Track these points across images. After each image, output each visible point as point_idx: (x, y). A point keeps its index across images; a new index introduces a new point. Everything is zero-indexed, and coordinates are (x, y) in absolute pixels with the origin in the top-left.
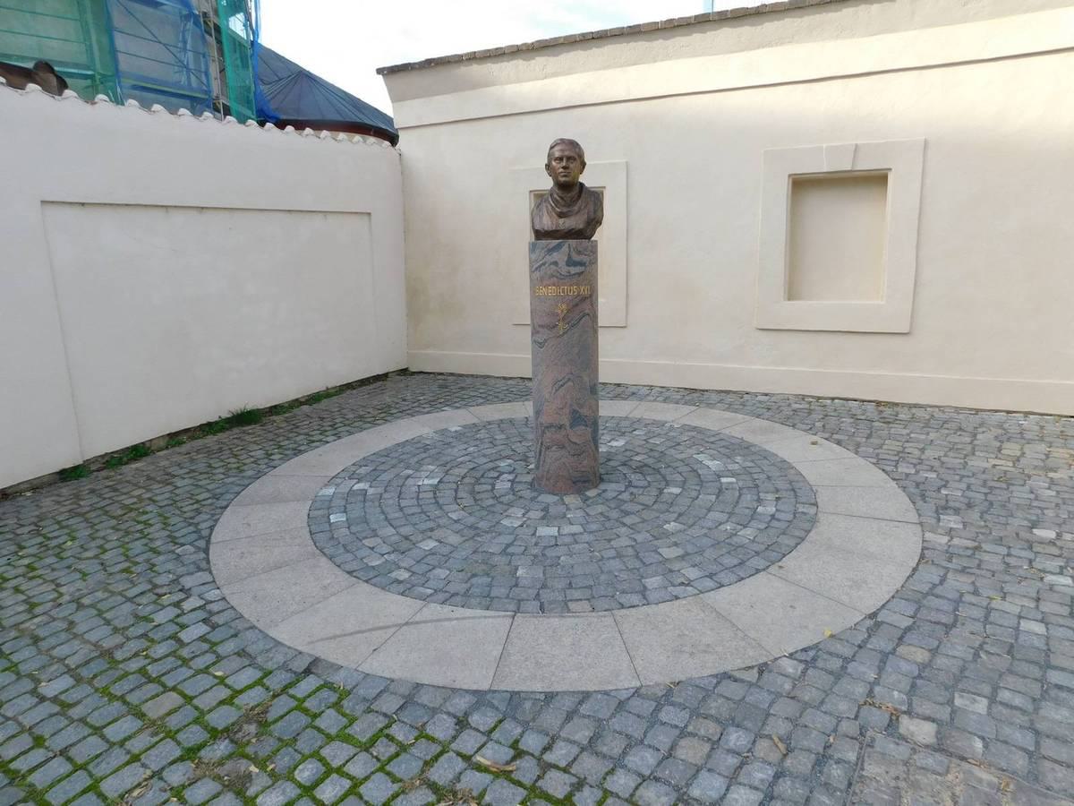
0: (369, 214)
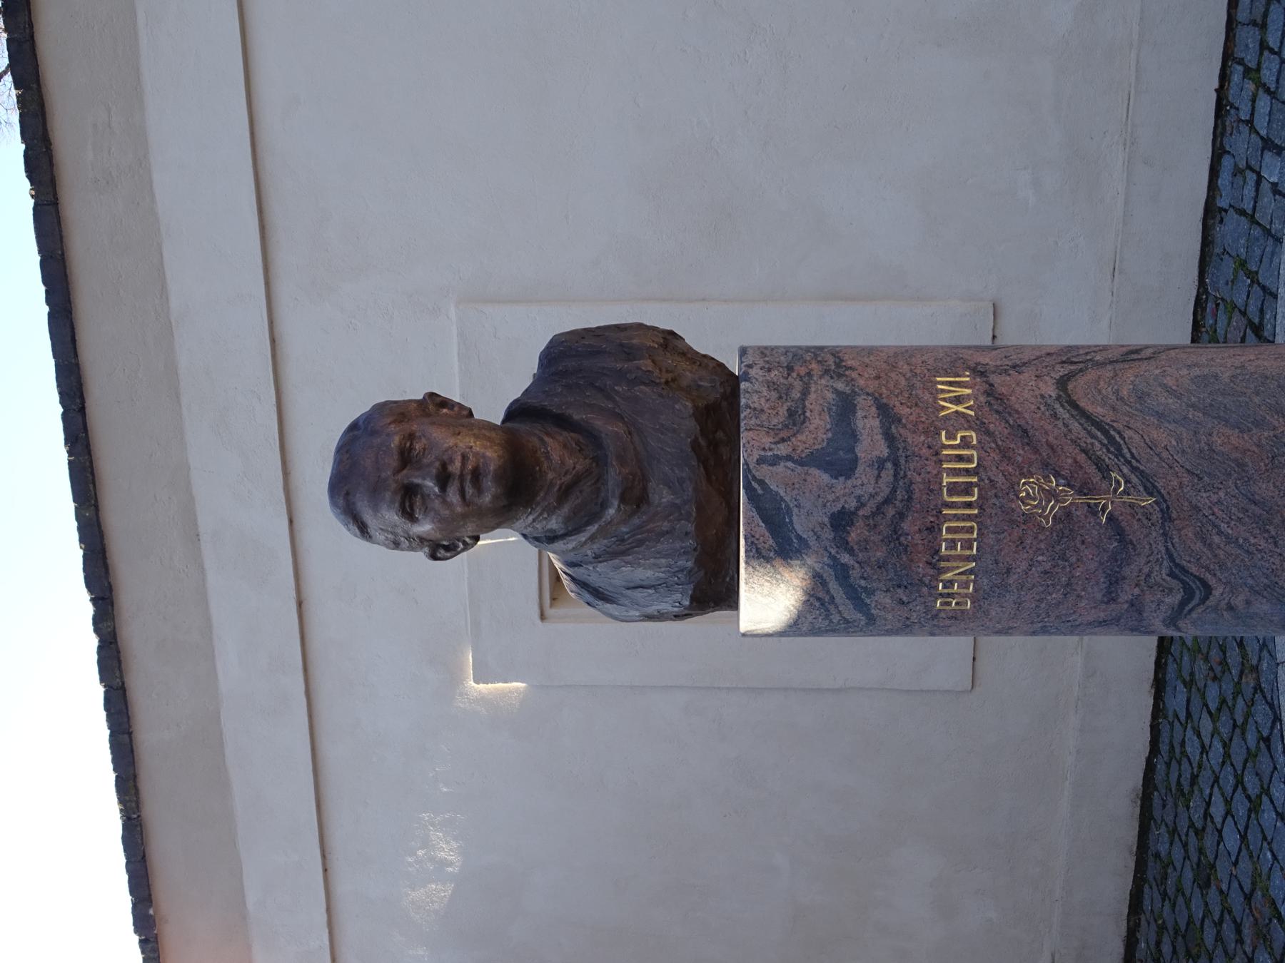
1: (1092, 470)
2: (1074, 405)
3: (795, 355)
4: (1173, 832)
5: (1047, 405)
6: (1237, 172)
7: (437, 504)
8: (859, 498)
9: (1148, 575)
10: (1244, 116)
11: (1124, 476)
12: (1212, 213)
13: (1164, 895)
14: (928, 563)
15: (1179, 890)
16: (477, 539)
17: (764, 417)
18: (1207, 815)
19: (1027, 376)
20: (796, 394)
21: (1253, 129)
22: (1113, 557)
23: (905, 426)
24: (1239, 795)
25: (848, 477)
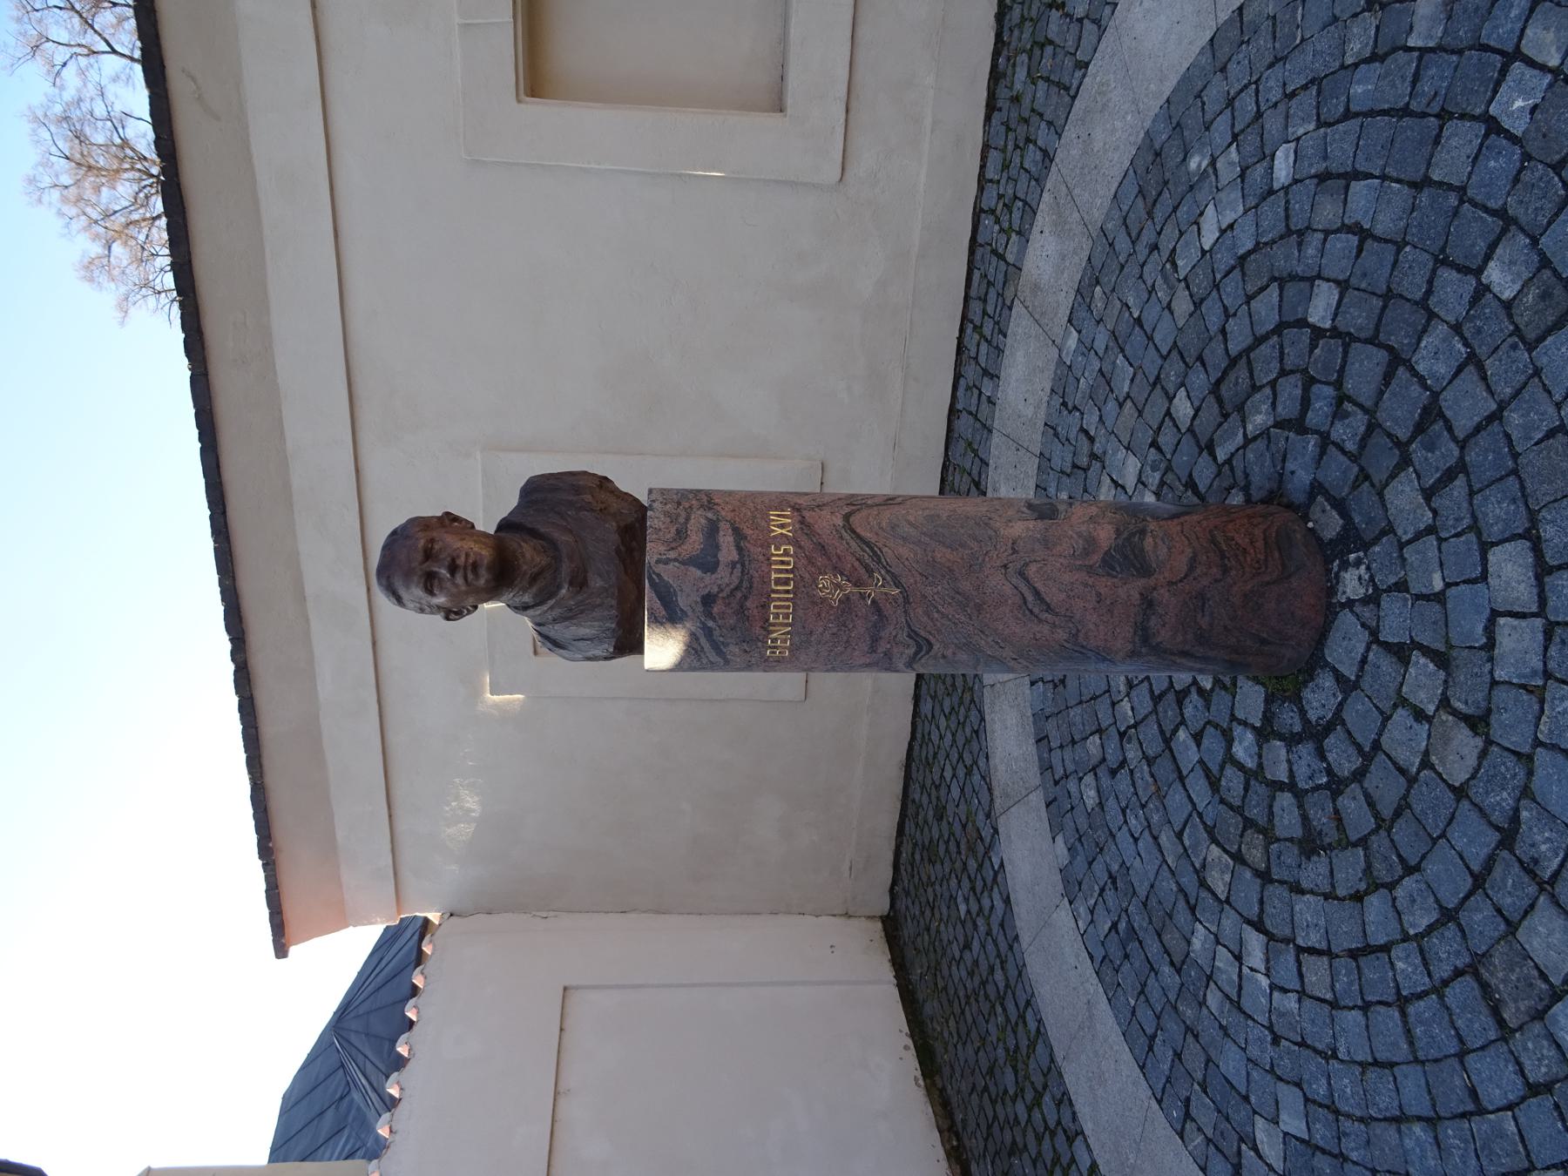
0: (565, 989)
1: (863, 571)
2: (854, 531)
3: (682, 495)
4: (923, 787)
5: (837, 530)
6: (968, 388)
7: (448, 585)
8: (719, 586)
9: (896, 636)
10: (973, 354)
11: (882, 576)
12: (953, 412)
13: (917, 825)
14: (762, 627)
15: (926, 822)
16: (476, 607)
17: (661, 533)
18: (942, 776)
19: (825, 512)
20: (682, 520)
21: (977, 363)
22: (875, 626)
23: (749, 542)
24: (960, 765)
25: (713, 573)
